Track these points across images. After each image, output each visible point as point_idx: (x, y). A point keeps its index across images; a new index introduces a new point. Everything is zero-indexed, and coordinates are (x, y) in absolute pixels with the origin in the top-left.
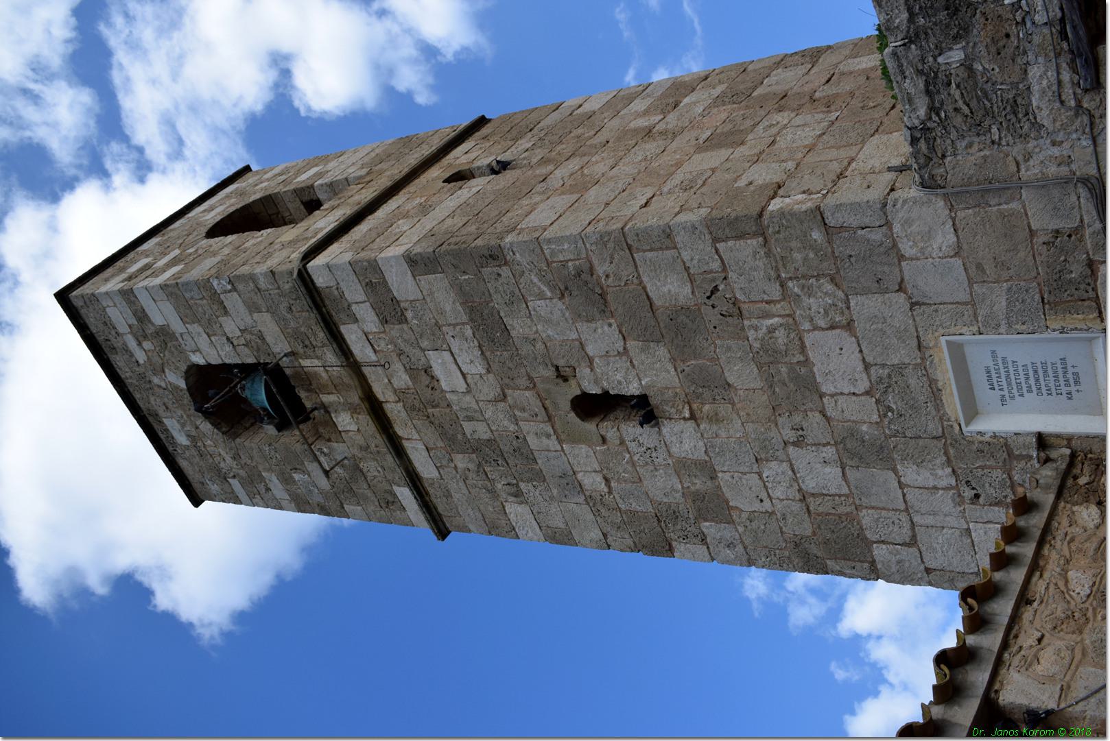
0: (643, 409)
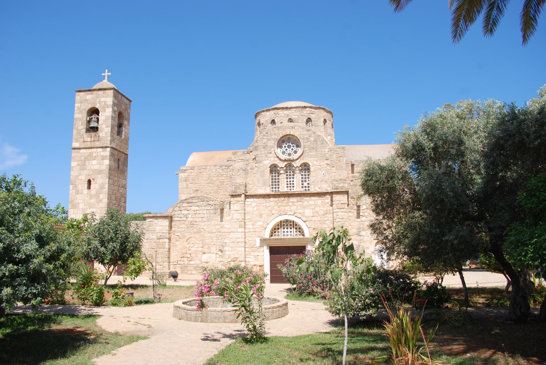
0: (89, 188)
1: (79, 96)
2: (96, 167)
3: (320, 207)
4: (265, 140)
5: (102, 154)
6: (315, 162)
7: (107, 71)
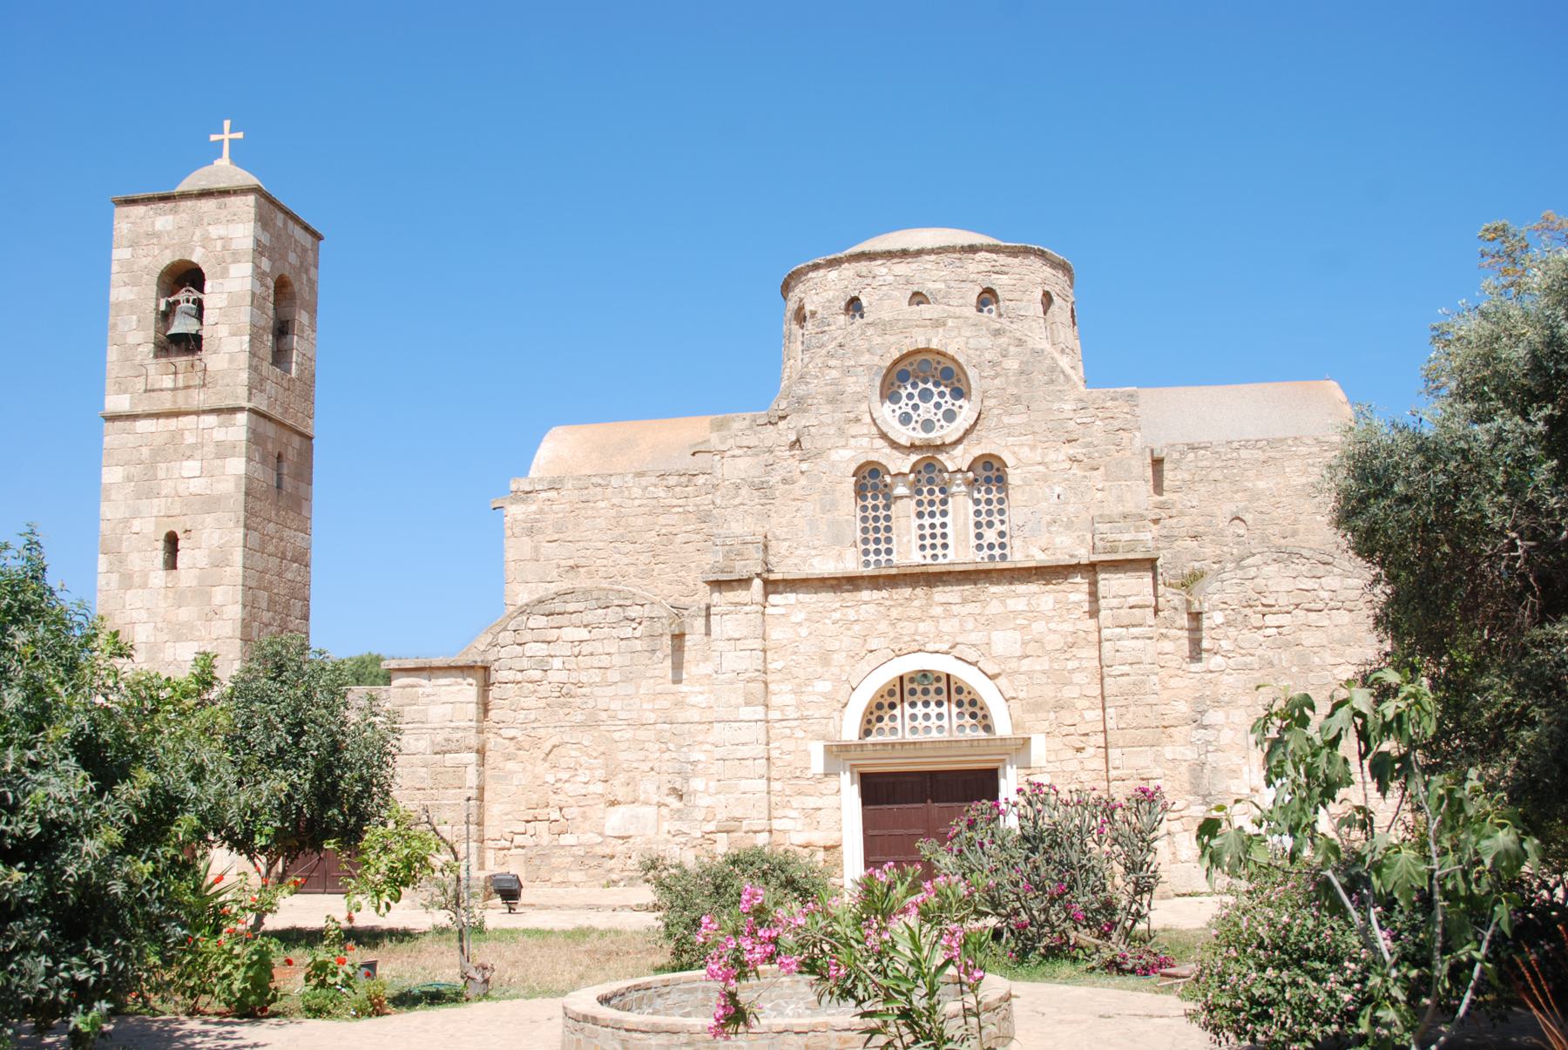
0: (171, 563)
1: (127, 221)
2: (196, 486)
3: (1049, 619)
4: (834, 373)
5: (219, 435)
6: (1025, 452)
7: (227, 124)
